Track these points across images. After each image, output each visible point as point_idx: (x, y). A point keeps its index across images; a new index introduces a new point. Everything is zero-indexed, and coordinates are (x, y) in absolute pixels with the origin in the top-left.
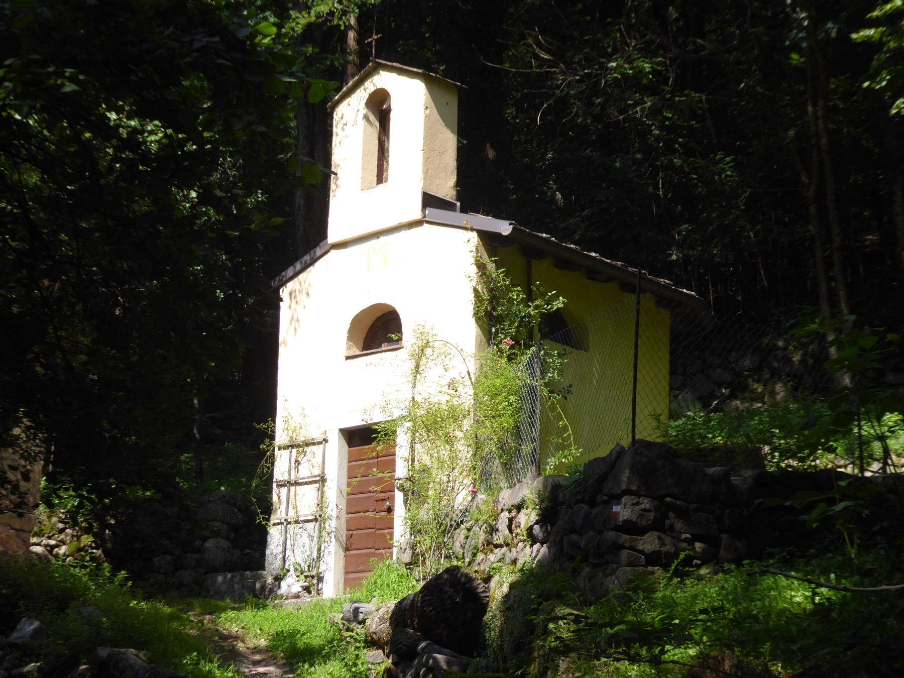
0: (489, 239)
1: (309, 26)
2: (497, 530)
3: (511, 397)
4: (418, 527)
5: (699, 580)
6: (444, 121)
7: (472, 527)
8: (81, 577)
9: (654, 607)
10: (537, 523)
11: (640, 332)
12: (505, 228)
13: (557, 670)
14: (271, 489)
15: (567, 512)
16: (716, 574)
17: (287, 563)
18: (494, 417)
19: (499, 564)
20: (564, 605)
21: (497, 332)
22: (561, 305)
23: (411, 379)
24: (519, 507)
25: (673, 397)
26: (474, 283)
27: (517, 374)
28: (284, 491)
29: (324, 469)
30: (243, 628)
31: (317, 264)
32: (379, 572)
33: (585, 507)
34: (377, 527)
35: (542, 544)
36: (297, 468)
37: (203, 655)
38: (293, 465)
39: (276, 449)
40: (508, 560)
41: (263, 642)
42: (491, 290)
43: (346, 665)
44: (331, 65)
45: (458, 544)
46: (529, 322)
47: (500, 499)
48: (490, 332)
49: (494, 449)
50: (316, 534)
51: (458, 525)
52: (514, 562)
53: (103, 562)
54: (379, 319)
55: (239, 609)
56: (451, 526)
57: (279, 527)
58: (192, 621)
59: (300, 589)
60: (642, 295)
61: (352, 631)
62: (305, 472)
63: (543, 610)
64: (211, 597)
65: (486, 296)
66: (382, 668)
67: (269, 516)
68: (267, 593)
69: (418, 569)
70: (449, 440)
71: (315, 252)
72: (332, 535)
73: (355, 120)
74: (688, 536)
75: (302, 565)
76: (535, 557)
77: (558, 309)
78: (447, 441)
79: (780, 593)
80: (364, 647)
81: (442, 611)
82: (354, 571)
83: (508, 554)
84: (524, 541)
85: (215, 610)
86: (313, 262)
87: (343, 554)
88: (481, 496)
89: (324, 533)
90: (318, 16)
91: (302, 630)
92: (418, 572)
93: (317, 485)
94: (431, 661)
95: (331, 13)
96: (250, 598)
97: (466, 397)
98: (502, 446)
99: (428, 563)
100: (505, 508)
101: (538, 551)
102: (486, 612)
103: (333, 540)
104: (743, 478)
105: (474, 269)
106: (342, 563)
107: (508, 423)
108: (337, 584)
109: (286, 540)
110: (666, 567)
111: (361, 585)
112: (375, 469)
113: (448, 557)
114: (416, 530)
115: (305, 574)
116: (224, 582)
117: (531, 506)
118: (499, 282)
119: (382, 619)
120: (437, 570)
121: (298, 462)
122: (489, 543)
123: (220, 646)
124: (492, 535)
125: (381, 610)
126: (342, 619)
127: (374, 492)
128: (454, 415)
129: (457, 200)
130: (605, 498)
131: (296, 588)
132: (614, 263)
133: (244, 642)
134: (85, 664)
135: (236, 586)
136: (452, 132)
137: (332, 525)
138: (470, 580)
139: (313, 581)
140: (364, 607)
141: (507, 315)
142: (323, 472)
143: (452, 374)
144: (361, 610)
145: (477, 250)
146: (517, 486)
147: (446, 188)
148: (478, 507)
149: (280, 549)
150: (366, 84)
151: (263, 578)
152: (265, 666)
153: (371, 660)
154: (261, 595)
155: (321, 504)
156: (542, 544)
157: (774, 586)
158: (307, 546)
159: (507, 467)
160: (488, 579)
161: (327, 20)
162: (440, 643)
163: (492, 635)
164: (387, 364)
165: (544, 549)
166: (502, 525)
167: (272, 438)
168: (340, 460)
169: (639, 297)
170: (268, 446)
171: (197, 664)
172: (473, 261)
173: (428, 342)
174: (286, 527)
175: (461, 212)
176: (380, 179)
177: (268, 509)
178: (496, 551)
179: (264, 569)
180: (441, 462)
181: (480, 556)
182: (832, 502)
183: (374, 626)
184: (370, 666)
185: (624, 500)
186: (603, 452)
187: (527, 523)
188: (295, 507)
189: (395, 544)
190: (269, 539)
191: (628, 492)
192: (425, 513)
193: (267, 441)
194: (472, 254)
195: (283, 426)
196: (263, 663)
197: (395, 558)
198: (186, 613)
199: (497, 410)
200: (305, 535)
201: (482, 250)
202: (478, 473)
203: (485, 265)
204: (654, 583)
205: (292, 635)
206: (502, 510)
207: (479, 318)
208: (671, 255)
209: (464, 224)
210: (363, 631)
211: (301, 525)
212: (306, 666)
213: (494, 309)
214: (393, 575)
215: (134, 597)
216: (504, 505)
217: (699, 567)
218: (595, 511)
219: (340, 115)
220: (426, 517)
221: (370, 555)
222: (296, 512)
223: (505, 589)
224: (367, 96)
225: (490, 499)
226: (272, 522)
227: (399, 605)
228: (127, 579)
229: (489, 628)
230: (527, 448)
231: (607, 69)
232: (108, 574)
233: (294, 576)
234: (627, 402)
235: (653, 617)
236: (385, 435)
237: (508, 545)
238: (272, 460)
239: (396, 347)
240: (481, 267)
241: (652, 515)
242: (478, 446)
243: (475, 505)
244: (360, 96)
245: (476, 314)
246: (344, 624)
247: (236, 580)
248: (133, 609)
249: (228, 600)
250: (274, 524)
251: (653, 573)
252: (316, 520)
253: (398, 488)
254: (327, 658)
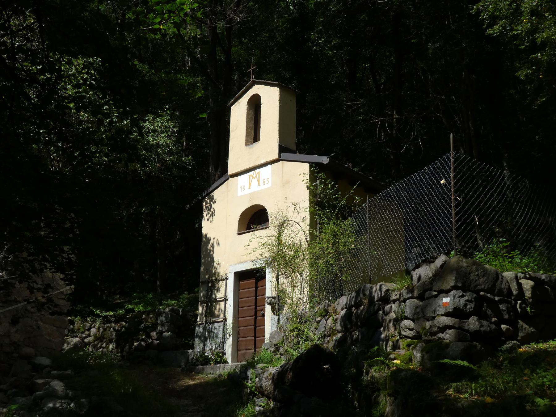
12: (325, 160)
176: (249, 188)
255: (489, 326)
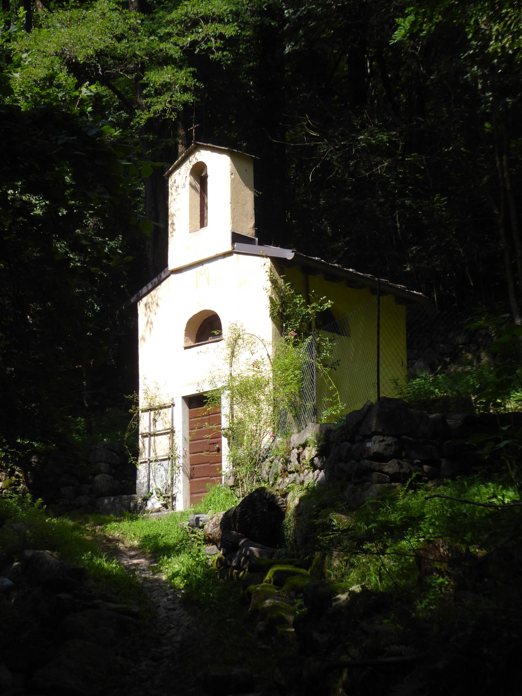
0: (278, 263)
1: (149, 120)
2: (290, 461)
3: (296, 371)
4: (238, 461)
5: (427, 491)
6: (244, 183)
7: (273, 460)
8: (12, 504)
9: (395, 510)
10: (316, 456)
11: (381, 324)
12: (289, 255)
13: (332, 556)
14: (138, 438)
15: (338, 447)
16: (438, 486)
17: (151, 489)
18: (285, 386)
19: (292, 484)
20: (335, 511)
21: (287, 327)
22: (330, 306)
23: (228, 361)
24: (304, 446)
25: (410, 365)
26: (269, 293)
27: (300, 354)
28: (147, 440)
29: (173, 424)
30: (122, 534)
31: (164, 284)
32: (212, 492)
33: (348, 444)
34: (211, 462)
35: (320, 470)
36: (155, 424)
37: (96, 553)
38: (152, 422)
39: (140, 412)
40: (298, 482)
41: (136, 543)
42: (281, 298)
43: (192, 556)
44: (163, 147)
45: (264, 472)
46: (309, 319)
47: (291, 441)
48: (282, 327)
49: (286, 407)
50: (170, 469)
51: (264, 459)
52: (302, 483)
53: (27, 493)
54: (205, 321)
55: (119, 521)
56: (260, 460)
57: (144, 464)
58: (88, 530)
59: (161, 506)
60: (381, 298)
61: (196, 534)
62: (160, 427)
63: (321, 515)
64: (101, 513)
65: (278, 302)
66: (216, 558)
67: (138, 458)
68: (138, 509)
69: (238, 489)
70: (256, 402)
71: (161, 276)
72: (181, 468)
73: (184, 184)
74: (419, 461)
75: (161, 489)
76: (316, 479)
77: (328, 309)
78: (254, 403)
79: (481, 497)
80: (204, 544)
81: (255, 518)
82: (196, 492)
83: (298, 478)
84: (308, 468)
85: (104, 522)
86: (160, 282)
87: (189, 481)
88: (279, 439)
89: (175, 467)
90: (155, 113)
91: (162, 534)
92: (239, 492)
93: (169, 435)
94: (248, 552)
95: (164, 111)
96: (126, 513)
97: (267, 371)
98: (293, 405)
99: (245, 485)
100: (295, 447)
101: (318, 475)
102: (284, 518)
103: (181, 472)
104: (454, 421)
105: (269, 284)
106: (188, 487)
107: (294, 389)
108: (185, 502)
109: (149, 473)
110: (403, 483)
111: (200, 502)
112: (206, 423)
113: (258, 481)
114: (236, 463)
115: (163, 495)
116: (109, 503)
117: (312, 445)
118: (286, 292)
119: (215, 525)
120: (251, 490)
121: (155, 420)
122: (285, 470)
123: (108, 546)
124: (287, 465)
125: (214, 519)
126: (189, 525)
127: (208, 438)
128: (259, 385)
129: (256, 236)
130: (361, 438)
131: (158, 505)
132: (366, 275)
133: (123, 544)
134: (17, 561)
135: (117, 505)
136: (250, 189)
137: (180, 461)
138: (273, 497)
139: (169, 500)
140: (203, 517)
141: (293, 315)
142: (172, 426)
143: (256, 357)
144: (201, 519)
145: (271, 271)
146: (302, 432)
147: (248, 229)
148: (276, 447)
149: (146, 479)
150: (191, 158)
151: (135, 499)
152: (138, 559)
153: (208, 552)
154: (134, 511)
155: (172, 448)
156: (320, 470)
157: (477, 493)
158: (164, 477)
159: (297, 417)
160: (285, 495)
161: (161, 116)
162: (254, 540)
163: (289, 533)
164: (213, 352)
165: (322, 474)
166: (293, 458)
167: (137, 404)
168: (184, 418)
169: (379, 300)
170: (134, 410)
171: (92, 559)
172: (268, 278)
173: (239, 335)
174: (149, 464)
175: (259, 244)
177: (136, 453)
178: (290, 476)
179: (135, 493)
180: (251, 417)
181: (280, 480)
182: (499, 441)
183: (210, 530)
184: (208, 556)
185: (374, 438)
186: (359, 406)
187: (310, 456)
188: (155, 451)
189: (223, 473)
190: (138, 473)
191: (376, 433)
192: (242, 452)
193: (133, 407)
194: (267, 273)
195: (144, 396)
196: (136, 557)
197: (223, 483)
198: (84, 525)
199: (287, 380)
200: (162, 469)
201: (274, 270)
202: (276, 424)
203: (276, 280)
204: (396, 495)
205: (155, 537)
206: (293, 448)
207: (274, 317)
208: (406, 267)
209: (261, 253)
210: (202, 533)
211: (159, 463)
212: (165, 558)
213: (284, 311)
214: (222, 495)
215: (48, 516)
216: (294, 444)
217: (426, 482)
218: (354, 447)
219: (173, 181)
220: (242, 455)
221: (206, 481)
222: (156, 454)
223: (297, 501)
224: (191, 167)
225: (285, 441)
226: (139, 461)
227: (225, 515)
228: (43, 504)
229: (287, 528)
230: (309, 405)
231: (358, 140)
232: (30, 501)
233: (157, 498)
234: (380, 370)
235: (395, 517)
236: (213, 400)
237: (298, 471)
238: (137, 420)
239: (219, 339)
240: (274, 282)
241: (393, 448)
242: (275, 404)
243: (275, 445)
244: (186, 168)
245: (272, 315)
246: (189, 529)
247: (117, 501)
248: (49, 523)
249: (112, 515)
250: (141, 463)
251: (395, 487)
252: (169, 459)
253: (223, 435)
254: (178, 552)
255: (409, 467)
